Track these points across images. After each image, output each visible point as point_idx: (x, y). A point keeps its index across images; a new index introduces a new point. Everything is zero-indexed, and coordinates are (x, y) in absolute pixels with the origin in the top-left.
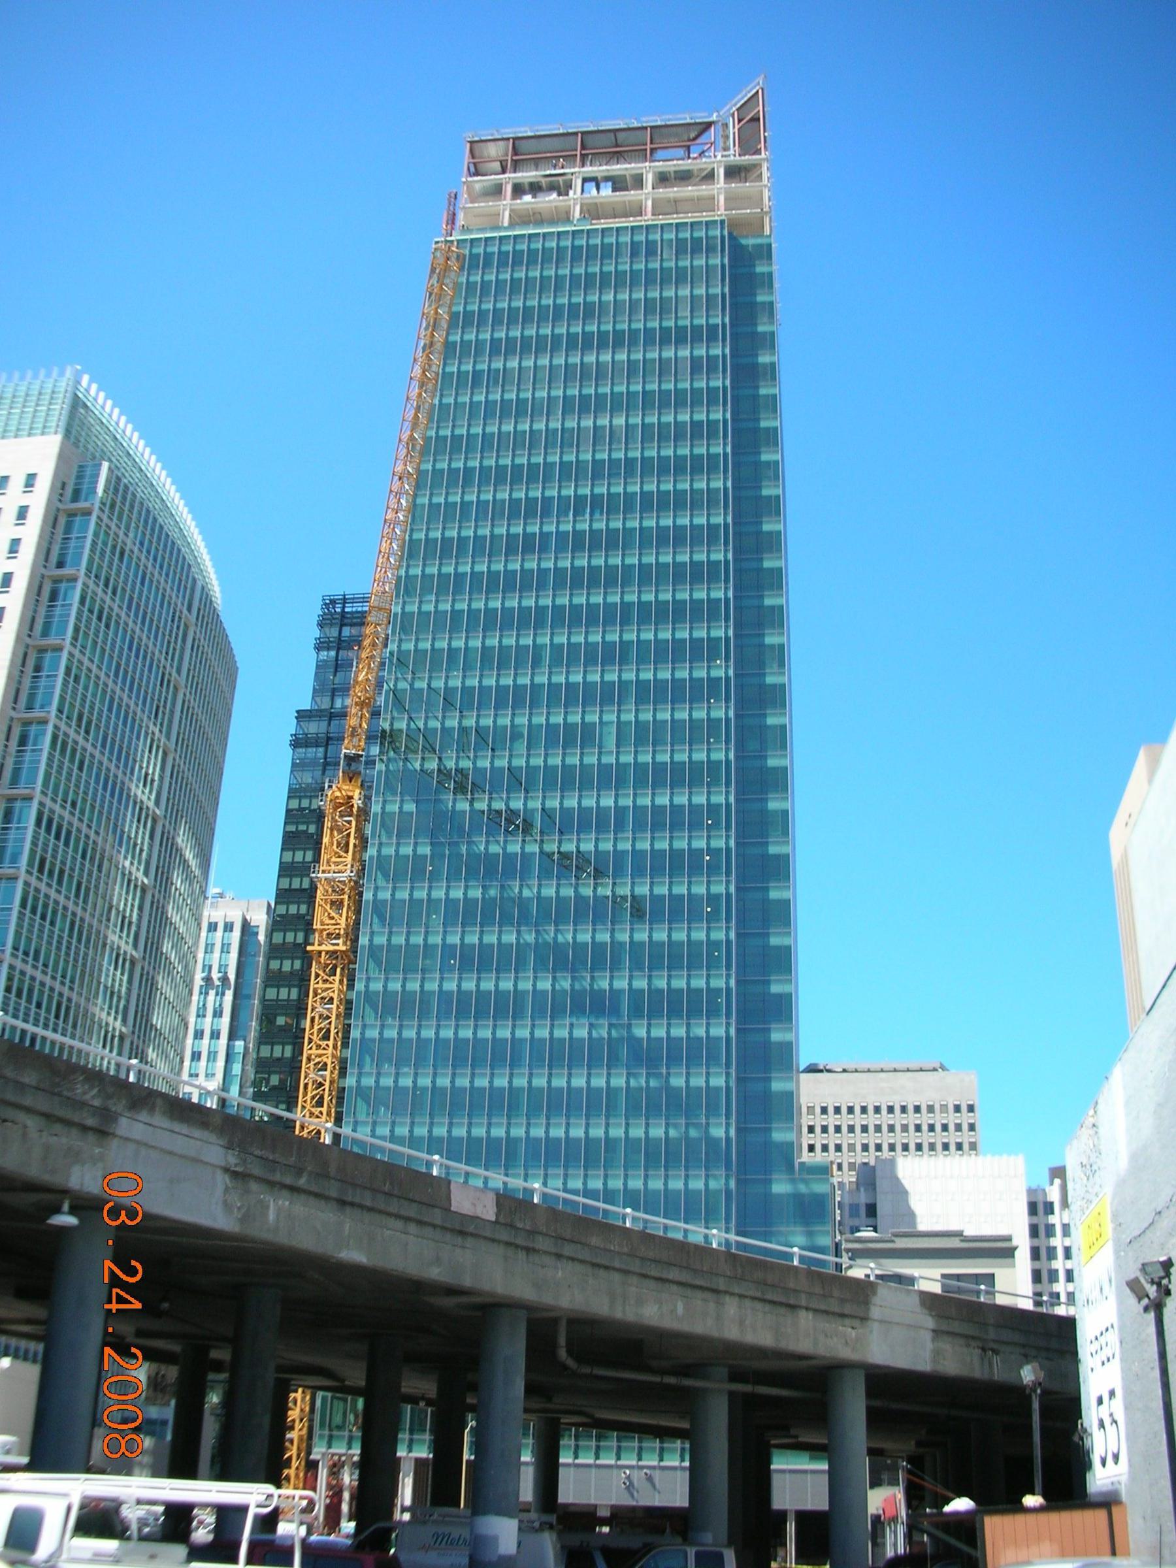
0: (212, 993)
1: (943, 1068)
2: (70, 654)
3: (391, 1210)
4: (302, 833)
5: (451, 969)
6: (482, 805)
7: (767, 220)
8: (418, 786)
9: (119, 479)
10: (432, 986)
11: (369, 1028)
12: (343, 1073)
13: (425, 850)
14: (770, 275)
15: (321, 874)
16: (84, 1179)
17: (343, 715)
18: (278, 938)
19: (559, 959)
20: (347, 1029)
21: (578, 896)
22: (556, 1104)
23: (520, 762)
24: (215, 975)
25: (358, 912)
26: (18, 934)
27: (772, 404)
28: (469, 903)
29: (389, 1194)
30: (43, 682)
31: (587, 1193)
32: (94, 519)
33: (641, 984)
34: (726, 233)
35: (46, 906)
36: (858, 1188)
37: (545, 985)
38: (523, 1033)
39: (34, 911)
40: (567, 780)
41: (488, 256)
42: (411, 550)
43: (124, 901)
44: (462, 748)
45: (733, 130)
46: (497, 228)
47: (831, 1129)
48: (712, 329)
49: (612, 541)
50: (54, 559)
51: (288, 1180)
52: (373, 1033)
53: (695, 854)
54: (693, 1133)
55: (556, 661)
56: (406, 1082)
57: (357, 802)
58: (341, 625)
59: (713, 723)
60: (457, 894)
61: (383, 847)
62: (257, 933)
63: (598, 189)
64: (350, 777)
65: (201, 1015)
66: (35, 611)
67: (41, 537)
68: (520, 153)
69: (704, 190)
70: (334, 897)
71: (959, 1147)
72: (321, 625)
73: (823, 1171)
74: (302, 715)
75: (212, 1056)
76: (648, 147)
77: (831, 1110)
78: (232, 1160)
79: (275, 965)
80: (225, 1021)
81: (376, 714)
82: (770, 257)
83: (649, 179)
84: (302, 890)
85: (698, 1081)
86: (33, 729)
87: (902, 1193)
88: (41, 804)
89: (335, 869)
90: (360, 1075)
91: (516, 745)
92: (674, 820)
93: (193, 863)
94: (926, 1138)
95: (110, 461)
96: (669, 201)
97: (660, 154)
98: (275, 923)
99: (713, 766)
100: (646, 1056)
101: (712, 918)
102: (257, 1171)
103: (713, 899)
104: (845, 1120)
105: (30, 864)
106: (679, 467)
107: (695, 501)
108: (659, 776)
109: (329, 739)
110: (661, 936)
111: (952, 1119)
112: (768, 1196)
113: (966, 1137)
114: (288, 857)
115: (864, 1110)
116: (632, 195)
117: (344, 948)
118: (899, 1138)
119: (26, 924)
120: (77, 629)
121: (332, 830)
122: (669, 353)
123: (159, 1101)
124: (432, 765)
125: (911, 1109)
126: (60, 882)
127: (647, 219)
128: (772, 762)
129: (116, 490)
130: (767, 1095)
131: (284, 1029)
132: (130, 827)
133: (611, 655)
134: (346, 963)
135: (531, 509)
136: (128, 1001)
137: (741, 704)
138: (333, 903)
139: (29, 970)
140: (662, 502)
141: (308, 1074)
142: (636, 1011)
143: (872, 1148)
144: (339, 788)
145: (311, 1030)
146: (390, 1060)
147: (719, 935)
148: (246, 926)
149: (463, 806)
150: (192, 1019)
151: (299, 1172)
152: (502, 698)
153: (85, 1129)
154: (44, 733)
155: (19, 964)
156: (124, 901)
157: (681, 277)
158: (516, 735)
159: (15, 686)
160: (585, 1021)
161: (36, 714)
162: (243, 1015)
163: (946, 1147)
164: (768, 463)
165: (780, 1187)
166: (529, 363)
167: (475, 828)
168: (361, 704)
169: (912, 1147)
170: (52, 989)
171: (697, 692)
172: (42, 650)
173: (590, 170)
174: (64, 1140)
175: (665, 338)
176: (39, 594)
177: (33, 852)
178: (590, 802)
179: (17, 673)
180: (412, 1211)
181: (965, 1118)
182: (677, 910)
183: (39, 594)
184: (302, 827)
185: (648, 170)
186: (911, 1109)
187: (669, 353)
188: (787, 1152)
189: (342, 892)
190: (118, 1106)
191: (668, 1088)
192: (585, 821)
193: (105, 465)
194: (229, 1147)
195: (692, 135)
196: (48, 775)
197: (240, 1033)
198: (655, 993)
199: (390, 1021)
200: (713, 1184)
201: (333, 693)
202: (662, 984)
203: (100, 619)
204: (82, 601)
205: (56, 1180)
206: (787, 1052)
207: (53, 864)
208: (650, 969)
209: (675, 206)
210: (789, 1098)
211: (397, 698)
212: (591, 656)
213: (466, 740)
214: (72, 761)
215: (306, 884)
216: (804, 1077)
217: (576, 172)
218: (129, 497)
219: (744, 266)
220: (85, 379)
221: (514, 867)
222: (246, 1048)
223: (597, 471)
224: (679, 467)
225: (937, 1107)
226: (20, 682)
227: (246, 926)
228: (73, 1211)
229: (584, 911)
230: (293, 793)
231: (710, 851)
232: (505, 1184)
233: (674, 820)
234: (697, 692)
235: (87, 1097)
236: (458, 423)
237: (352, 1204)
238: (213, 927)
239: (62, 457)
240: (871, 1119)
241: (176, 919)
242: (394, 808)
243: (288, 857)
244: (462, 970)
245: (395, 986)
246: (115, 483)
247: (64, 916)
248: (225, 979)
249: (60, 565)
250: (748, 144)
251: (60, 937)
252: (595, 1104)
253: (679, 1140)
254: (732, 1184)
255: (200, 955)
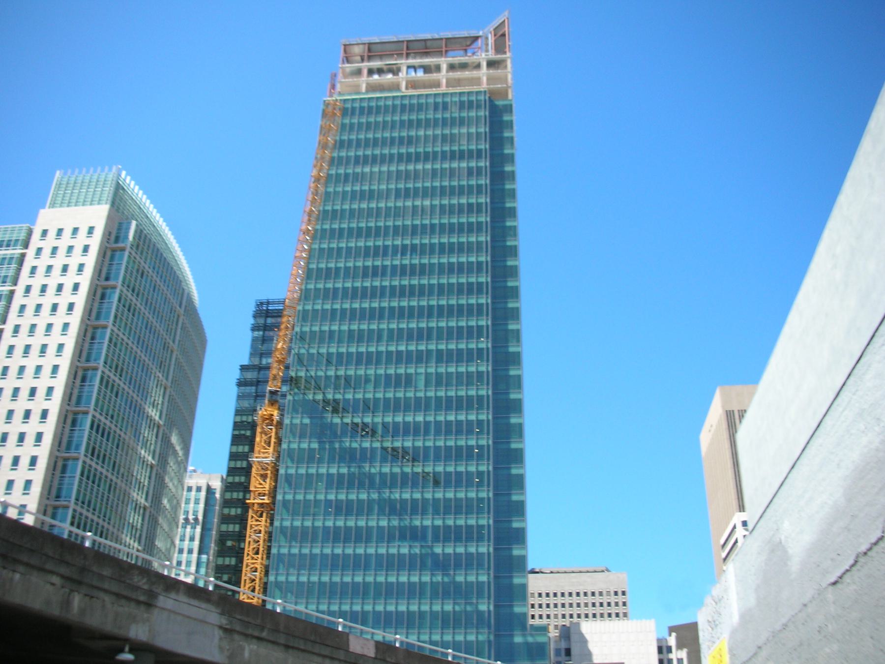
0: (189, 527)
1: (608, 570)
2: (112, 330)
3: (315, 651)
4: (244, 435)
5: (329, 514)
6: (348, 420)
7: (510, 91)
8: (312, 409)
9: (141, 231)
10: (319, 524)
11: (281, 548)
12: (267, 573)
13: (315, 446)
14: (512, 121)
15: (254, 459)
16: (138, 632)
17: (268, 368)
18: (228, 496)
19: (392, 508)
20: (269, 548)
21: (403, 473)
22: (390, 591)
23: (370, 396)
24: (191, 517)
25: (276, 481)
26: (79, 491)
27: (513, 194)
28: (340, 476)
29: (314, 642)
30: (96, 346)
31: (431, 643)
32: (127, 254)
33: (439, 522)
34: (487, 98)
35: (95, 475)
36: (560, 640)
37: (384, 523)
38: (371, 551)
39: (88, 478)
40: (396, 406)
41: (353, 109)
42: (309, 274)
43: (142, 476)
44: (336, 388)
45: (491, 40)
46: (359, 93)
47: (544, 606)
48: (479, 152)
49: (423, 270)
50: (104, 275)
51: (256, 634)
52: (284, 551)
53: (470, 448)
54: (469, 608)
55: (390, 338)
56: (304, 579)
57: (276, 417)
58: (267, 317)
59: (480, 374)
60: (333, 471)
61: (291, 444)
62: (214, 493)
63: (415, 71)
64: (272, 403)
65: (182, 540)
66: (92, 305)
67: (97, 263)
68: (372, 51)
69: (475, 74)
70: (262, 472)
71: (617, 615)
72: (255, 317)
73: (544, 629)
74: (243, 368)
75: (189, 563)
76: (444, 49)
77: (544, 595)
78: (224, 621)
79: (226, 511)
80: (196, 544)
81: (287, 368)
82: (511, 111)
83: (444, 67)
84: (243, 468)
85: (472, 578)
86: (90, 373)
87: (584, 641)
88: (94, 416)
89: (263, 456)
90: (277, 574)
91: (368, 386)
92: (459, 429)
93: (180, 453)
94: (598, 610)
95: (136, 220)
96: (455, 79)
97: (451, 53)
98: (227, 487)
99: (480, 398)
100: (441, 564)
101: (480, 484)
102: (238, 628)
103: (480, 474)
104: (552, 600)
105: (87, 450)
106: (461, 228)
107: (470, 248)
108: (449, 404)
109: (259, 382)
110: (450, 495)
111: (613, 599)
112: (512, 645)
113: (621, 609)
114: (234, 449)
115: (563, 594)
116: (434, 76)
117: (267, 501)
118: (583, 610)
119: (83, 486)
120: (116, 317)
121: (261, 433)
122: (455, 165)
123: (182, 586)
124: (319, 397)
125: (589, 594)
126: (103, 462)
127: (443, 89)
128: (513, 396)
129: (140, 237)
130: (511, 586)
131: (231, 548)
132: (146, 433)
133: (421, 335)
134: (269, 510)
135: (376, 252)
136: (141, 531)
137: (495, 363)
138: (262, 476)
139: (84, 512)
140: (451, 249)
141: (246, 574)
142: (436, 539)
143: (567, 616)
144: (265, 410)
145: (248, 549)
146: (294, 566)
147: (483, 495)
148: (210, 491)
149: (337, 420)
150: (177, 542)
151: (262, 628)
152: (359, 359)
153: (138, 602)
154: (96, 375)
155: (79, 509)
156: (142, 476)
157: (462, 122)
158: (367, 380)
159: (79, 347)
160: (406, 544)
161: (92, 364)
162: (207, 540)
163: (610, 615)
164: (510, 227)
165: (518, 639)
166: (376, 169)
167: (344, 433)
168: (279, 362)
169: (590, 615)
170: (98, 524)
171: (470, 356)
172: (95, 328)
173: (411, 61)
174: (126, 609)
175: (453, 156)
176: (94, 295)
177: (88, 444)
178: (409, 419)
179: (81, 340)
180: (326, 651)
181: (620, 599)
182: (458, 480)
183: (94, 295)
184: (243, 432)
185: (444, 62)
186: (589, 594)
187: (455, 165)
188: (521, 621)
189: (267, 469)
190: (158, 589)
191: (454, 583)
192: (407, 430)
193: (134, 223)
194: (222, 614)
195: (468, 43)
196: (97, 400)
197: (205, 550)
198: (447, 528)
199: (294, 543)
200: (481, 638)
201: (262, 355)
202: (450, 522)
203: (129, 310)
204: (119, 300)
205: (121, 633)
206: (523, 559)
207: (100, 451)
208: (444, 514)
209: (458, 82)
210: (524, 587)
211: (300, 359)
212: (410, 336)
213: (338, 383)
214: (112, 392)
215: (245, 464)
216: (531, 576)
217: (403, 62)
218: (147, 241)
219: (497, 115)
220: (124, 173)
221: (366, 456)
222: (208, 559)
223: (413, 231)
224: (461, 228)
225: (604, 593)
226: (82, 346)
227: (210, 491)
228: (131, 651)
229: (406, 481)
230: (238, 412)
231: (478, 447)
232: (384, 637)
233: (459, 429)
234: (470, 356)
235: (140, 584)
236: (462, 143)
237: (293, 648)
238: (190, 489)
239: (110, 218)
240: (567, 600)
241: (170, 485)
242: (297, 421)
243: (234, 449)
244: (336, 514)
245: (297, 523)
246: (139, 233)
247: (106, 481)
248: (196, 519)
249: (107, 279)
250: (500, 47)
251: (103, 493)
252: (413, 591)
253: (460, 612)
254: (492, 637)
255: (183, 505)
